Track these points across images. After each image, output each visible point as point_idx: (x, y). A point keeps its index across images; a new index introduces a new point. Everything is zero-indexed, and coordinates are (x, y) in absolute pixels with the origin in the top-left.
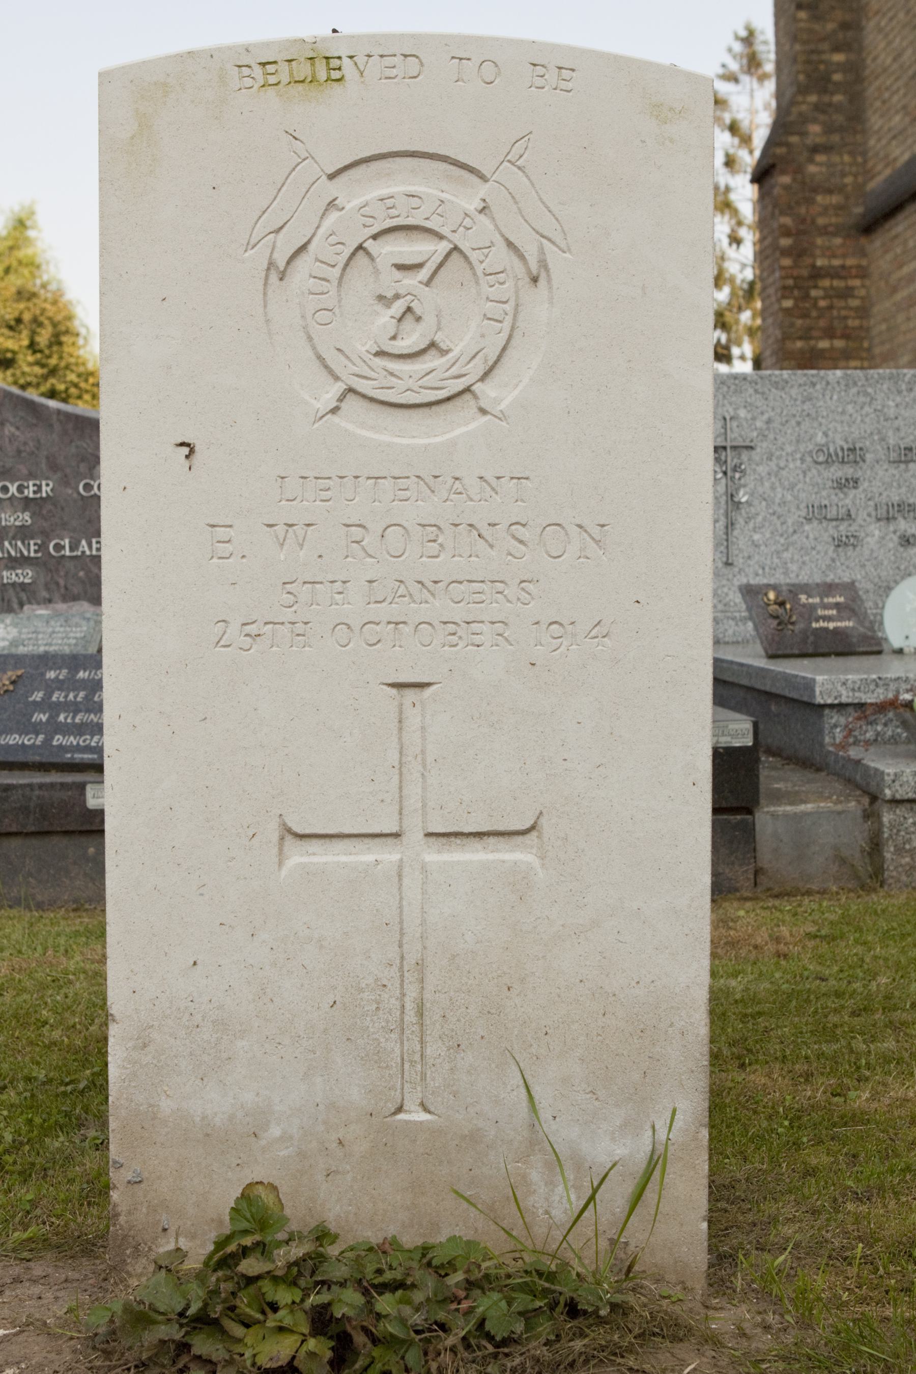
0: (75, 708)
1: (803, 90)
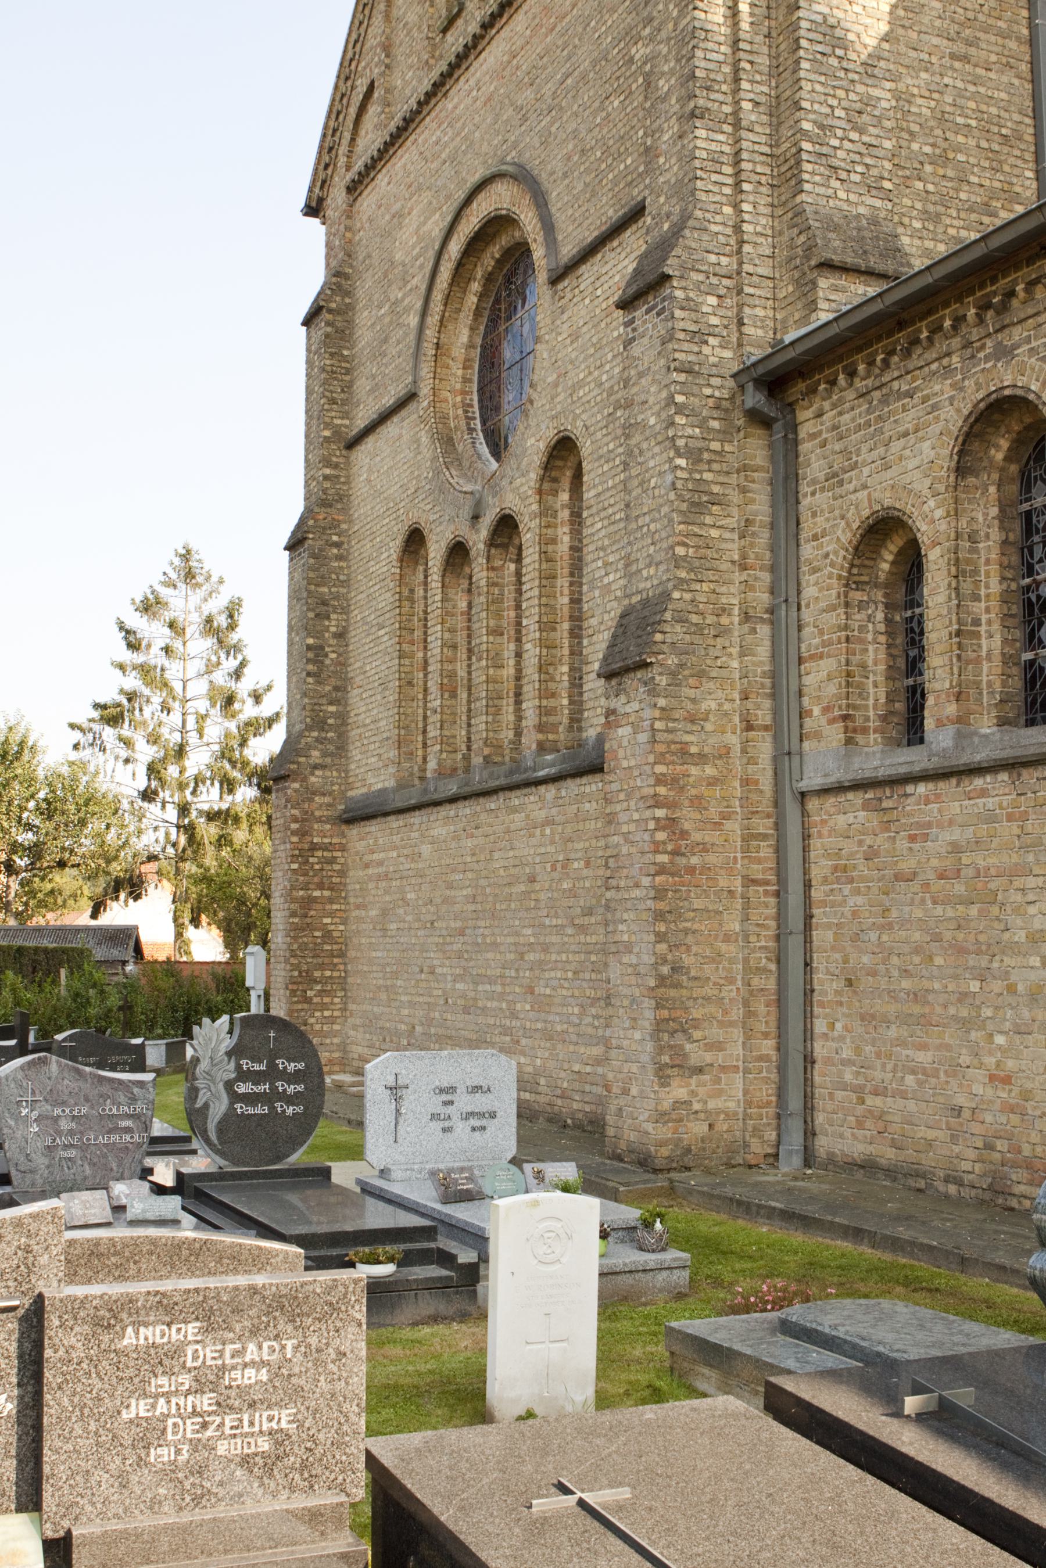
1: (309, 728)
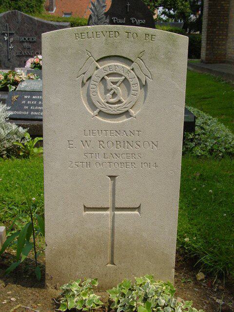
0: (35, 105)
